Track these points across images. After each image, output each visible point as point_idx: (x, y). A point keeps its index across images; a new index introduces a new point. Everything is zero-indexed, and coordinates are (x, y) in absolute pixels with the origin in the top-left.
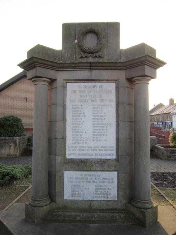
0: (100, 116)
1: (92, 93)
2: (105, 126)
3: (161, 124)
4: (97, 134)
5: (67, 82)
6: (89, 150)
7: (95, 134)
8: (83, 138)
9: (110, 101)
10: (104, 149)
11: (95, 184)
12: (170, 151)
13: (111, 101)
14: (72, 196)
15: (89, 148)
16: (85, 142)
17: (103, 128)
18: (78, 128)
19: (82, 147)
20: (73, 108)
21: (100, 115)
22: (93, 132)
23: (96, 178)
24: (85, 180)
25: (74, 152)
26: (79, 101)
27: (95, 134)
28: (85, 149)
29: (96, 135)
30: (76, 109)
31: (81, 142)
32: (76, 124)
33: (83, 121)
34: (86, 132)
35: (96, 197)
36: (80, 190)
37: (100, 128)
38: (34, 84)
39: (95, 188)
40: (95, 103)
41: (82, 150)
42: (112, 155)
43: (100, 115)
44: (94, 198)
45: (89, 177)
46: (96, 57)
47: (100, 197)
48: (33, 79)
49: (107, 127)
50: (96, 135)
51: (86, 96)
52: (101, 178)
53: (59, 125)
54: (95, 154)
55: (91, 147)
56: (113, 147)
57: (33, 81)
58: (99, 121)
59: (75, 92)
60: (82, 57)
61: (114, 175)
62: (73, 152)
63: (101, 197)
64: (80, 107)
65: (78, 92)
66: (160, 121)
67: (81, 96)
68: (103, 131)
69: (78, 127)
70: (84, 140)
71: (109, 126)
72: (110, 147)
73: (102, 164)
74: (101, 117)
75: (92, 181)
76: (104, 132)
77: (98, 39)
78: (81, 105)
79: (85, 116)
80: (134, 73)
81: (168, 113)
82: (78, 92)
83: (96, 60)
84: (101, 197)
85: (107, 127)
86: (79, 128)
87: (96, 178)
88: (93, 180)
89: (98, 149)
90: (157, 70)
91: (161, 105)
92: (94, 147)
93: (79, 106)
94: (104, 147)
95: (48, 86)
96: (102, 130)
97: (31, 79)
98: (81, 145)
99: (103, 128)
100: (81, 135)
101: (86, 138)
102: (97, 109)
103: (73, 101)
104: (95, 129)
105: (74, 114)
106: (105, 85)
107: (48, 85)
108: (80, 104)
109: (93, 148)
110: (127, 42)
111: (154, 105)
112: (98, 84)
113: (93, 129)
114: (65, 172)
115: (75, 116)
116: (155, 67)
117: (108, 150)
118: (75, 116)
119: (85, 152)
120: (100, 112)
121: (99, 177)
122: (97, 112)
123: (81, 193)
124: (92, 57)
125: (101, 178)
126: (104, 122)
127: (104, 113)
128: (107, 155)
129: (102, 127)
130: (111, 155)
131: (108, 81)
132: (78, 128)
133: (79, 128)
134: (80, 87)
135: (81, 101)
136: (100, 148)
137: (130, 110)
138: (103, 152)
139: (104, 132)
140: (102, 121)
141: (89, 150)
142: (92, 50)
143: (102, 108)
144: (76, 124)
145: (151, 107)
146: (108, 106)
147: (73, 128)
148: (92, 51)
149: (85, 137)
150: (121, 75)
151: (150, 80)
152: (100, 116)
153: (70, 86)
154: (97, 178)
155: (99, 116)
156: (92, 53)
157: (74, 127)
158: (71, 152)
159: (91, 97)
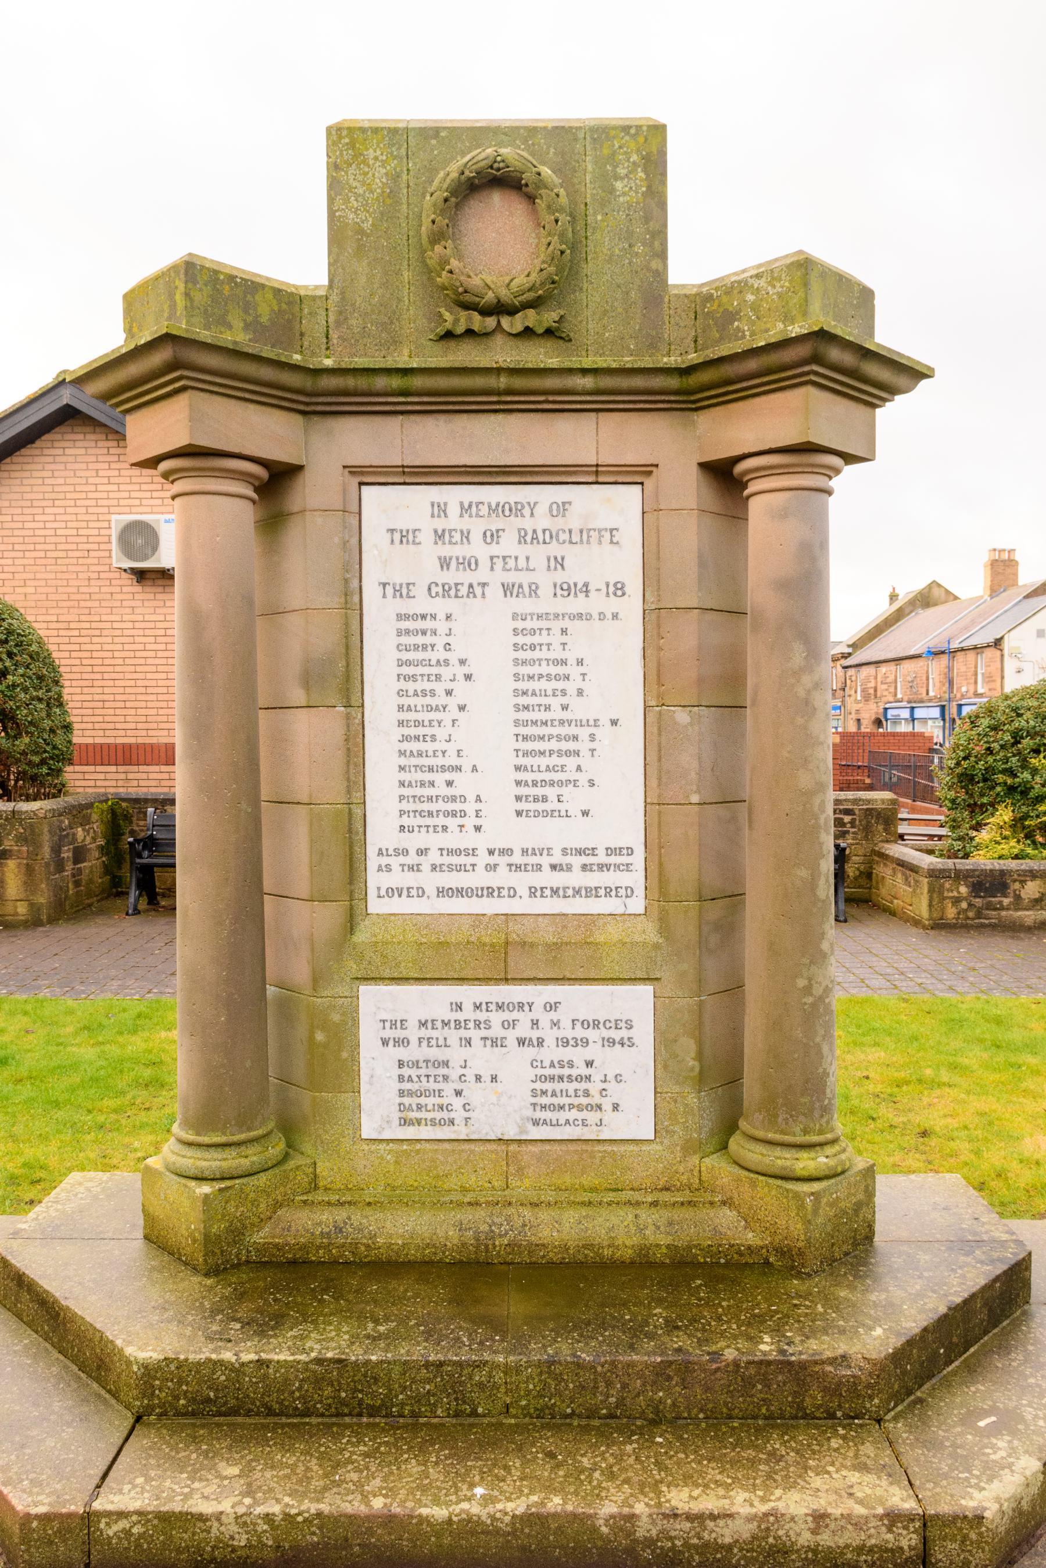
0: (557, 678)
1: (509, 545)
2: (584, 733)
3: (936, 712)
4: (538, 776)
5: (361, 484)
6: (496, 865)
7: (529, 777)
8: (463, 799)
9: (611, 589)
10: (577, 861)
11: (530, 1052)
12: (975, 880)
13: (619, 589)
14: (405, 1122)
15: (495, 859)
16: (470, 822)
17: (445, 1115)
18: (429, 747)
19: (457, 852)
20: (399, 633)
21: (554, 670)
22: (518, 768)
23: (535, 1023)
24: (475, 1034)
25: (409, 879)
26: (434, 590)
27: (529, 777)
28: (471, 860)
29: (535, 784)
30: (420, 640)
31: (452, 823)
32: (418, 723)
33: (462, 708)
34: (474, 769)
35: (536, 1123)
36: (448, 1089)
37: (554, 745)
38: (169, 494)
39: (531, 1073)
40: (525, 605)
41: (460, 868)
42: (622, 892)
43: (554, 670)
44: (529, 1126)
45: (496, 1018)
46: (528, 332)
47: (562, 1121)
48: (164, 466)
49: (592, 737)
50: (535, 784)
51: (470, 564)
52: (566, 1023)
53: (308, 735)
54: (533, 892)
55: (506, 852)
56: (630, 851)
57: (166, 475)
58: (548, 708)
59: (405, 537)
60: (449, 335)
61: (636, 1004)
62: (399, 890)
63: (567, 1122)
64: (442, 626)
65: (426, 537)
66: (930, 700)
67: (444, 563)
68: (571, 762)
69: (434, 738)
70: (464, 814)
71: (605, 732)
72: (610, 851)
73: (562, 954)
74: (560, 685)
75: (512, 1035)
76: (579, 768)
77: (531, 199)
78: (448, 617)
79: (468, 677)
80: (751, 427)
81: (975, 648)
82: (426, 537)
83: (540, 355)
84: (567, 1122)
85: (592, 737)
86: (436, 746)
87: (535, 1023)
88: (523, 1030)
89: (545, 861)
90: (882, 414)
91: (936, 592)
92: (525, 852)
93: (434, 617)
94: (580, 852)
95: (254, 502)
96: (568, 753)
97: (152, 463)
98: (453, 840)
99: (445, 1115)
100: (450, 784)
101: (478, 799)
102: (536, 639)
103: (402, 591)
104: (526, 754)
105: (409, 663)
106: (589, 503)
107: (255, 496)
108: (440, 606)
109: (517, 858)
110: (712, 242)
111: (893, 597)
112: (544, 496)
113: (517, 751)
114: (361, 988)
115: (413, 678)
116: (870, 399)
117: (601, 867)
118: (413, 678)
119: (479, 879)
120: (557, 653)
121: (553, 1016)
122: (537, 654)
123: (457, 1103)
124: (510, 334)
125: (566, 1023)
126: (580, 710)
127: (580, 662)
128: (592, 892)
129: (567, 738)
130: (623, 896)
131: (596, 474)
132: (429, 747)
133: (436, 746)
134: (440, 510)
135: (447, 591)
136: (557, 858)
137: (725, 647)
138: (576, 879)
139: (579, 768)
140: (565, 708)
141: (496, 865)
142: (511, 310)
143: (564, 631)
144: (418, 723)
145: (849, 610)
146: (602, 616)
147: (406, 746)
148: (505, 295)
149: (471, 797)
150: (674, 447)
151: (838, 471)
152: (557, 678)
153: (383, 507)
154: (545, 1020)
155: (559, 738)
156: (500, 309)
157: (405, 738)
158: (398, 878)
159: (505, 569)
